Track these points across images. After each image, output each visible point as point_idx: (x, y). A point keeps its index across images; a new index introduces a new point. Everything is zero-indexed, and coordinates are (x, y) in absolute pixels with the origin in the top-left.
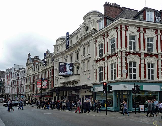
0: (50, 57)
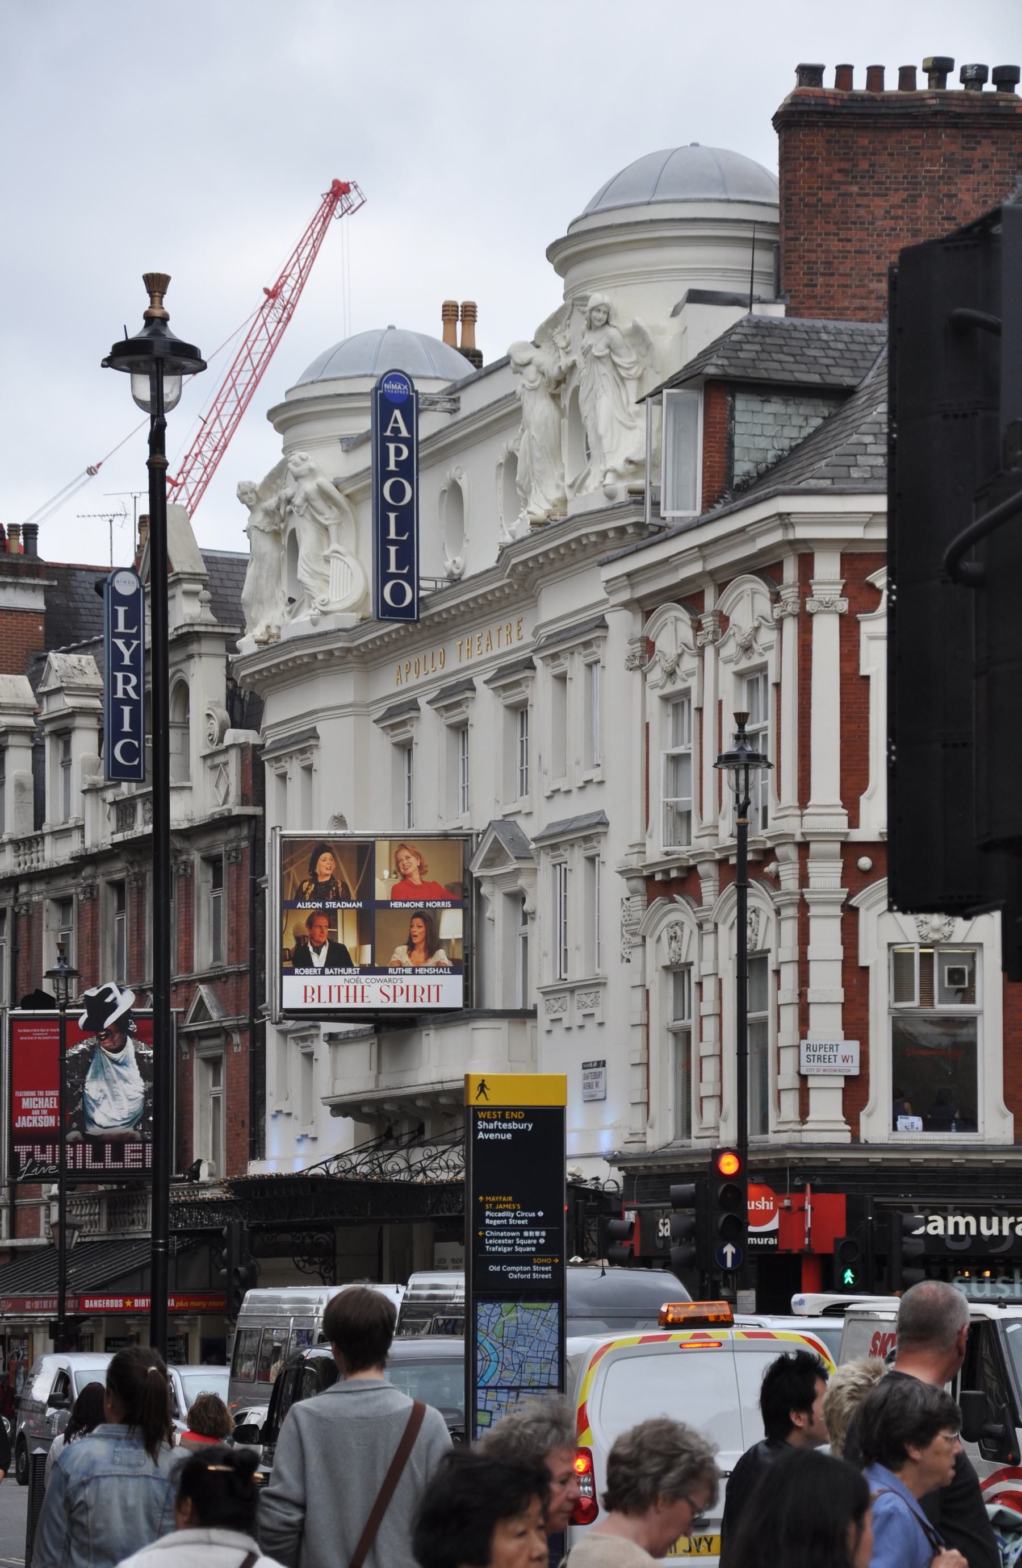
0: (206, 646)
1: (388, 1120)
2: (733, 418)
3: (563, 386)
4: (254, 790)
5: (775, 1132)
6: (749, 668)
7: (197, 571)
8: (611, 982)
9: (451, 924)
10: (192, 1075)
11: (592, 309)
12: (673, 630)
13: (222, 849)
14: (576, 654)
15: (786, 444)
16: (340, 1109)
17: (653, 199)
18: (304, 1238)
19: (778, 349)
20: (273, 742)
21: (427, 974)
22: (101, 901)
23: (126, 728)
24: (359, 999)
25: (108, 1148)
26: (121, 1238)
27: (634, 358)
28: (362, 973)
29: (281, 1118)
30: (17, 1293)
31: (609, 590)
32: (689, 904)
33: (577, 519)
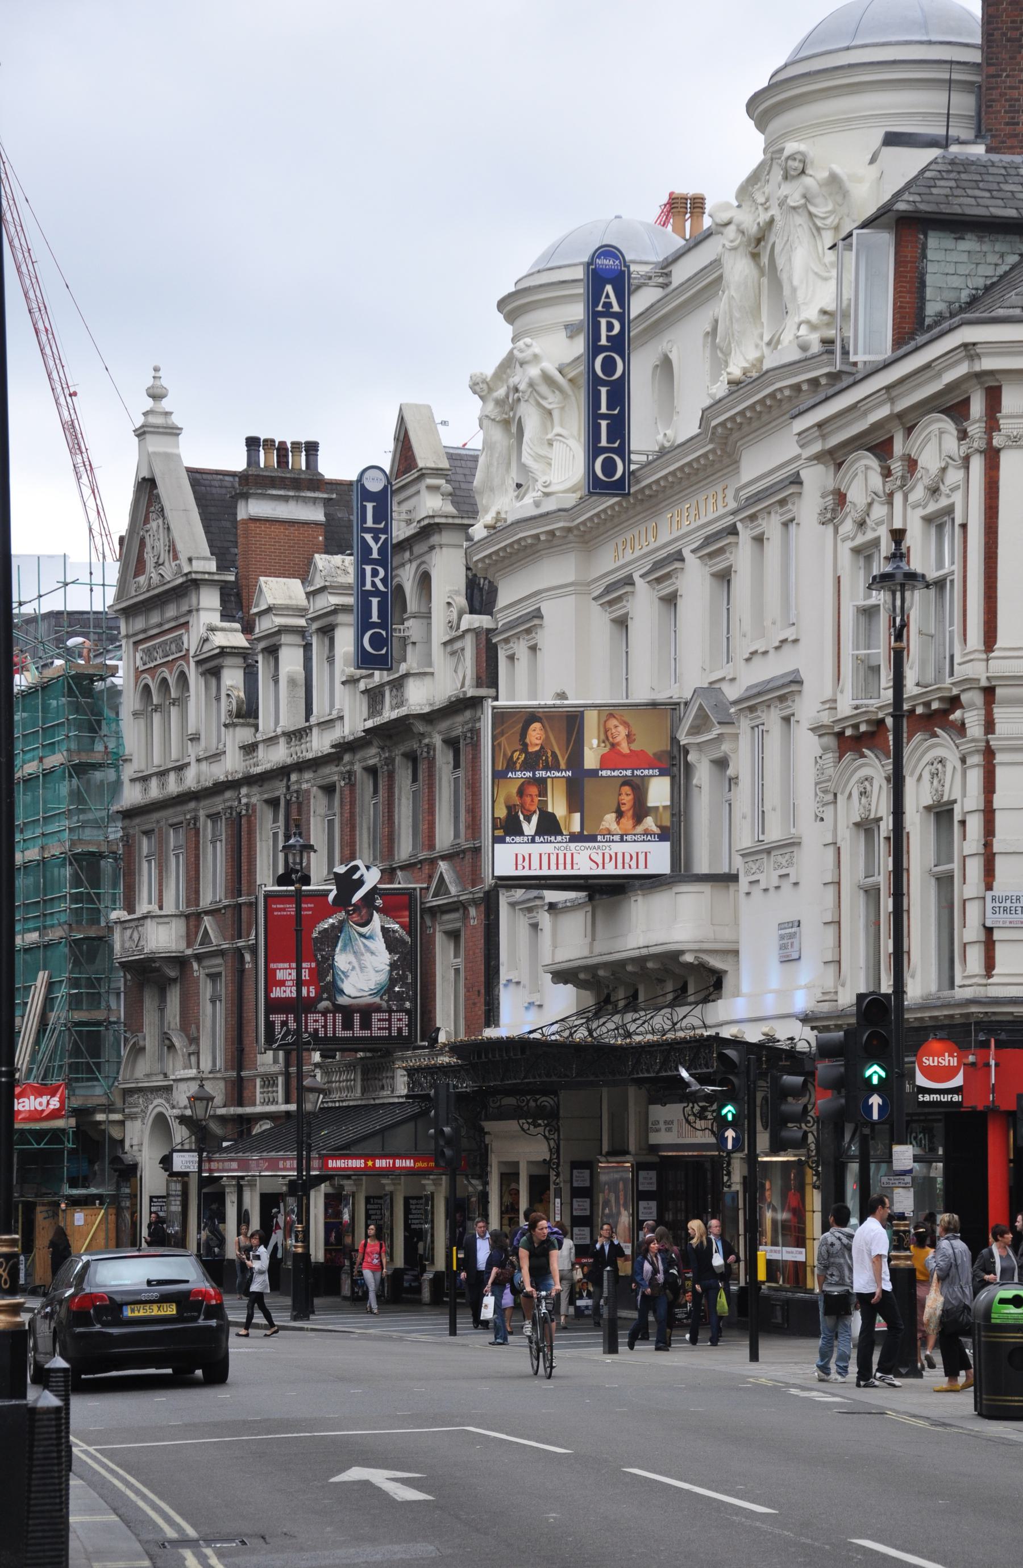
0: (445, 537)
1: (608, 985)
2: (924, 256)
3: (762, 243)
4: (488, 674)
5: (960, 987)
6: (937, 511)
7: (441, 466)
8: (805, 841)
9: (659, 792)
10: (434, 948)
11: (788, 158)
12: (864, 477)
13: (458, 731)
14: (773, 514)
15: (980, 283)
16: (562, 976)
17: (853, 44)
18: (528, 1101)
19: (974, 184)
20: (503, 625)
21: (635, 841)
22: (358, 786)
23: (375, 618)
24: (569, 866)
25: (357, 1017)
26: (372, 1102)
27: (830, 207)
28: (571, 841)
29: (512, 987)
30: (273, 1153)
31: (801, 443)
32: (877, 757)
33: (771, 373)
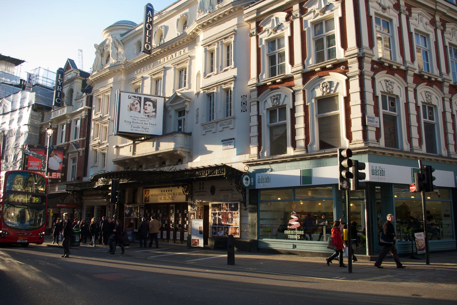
23: (59, 96)
